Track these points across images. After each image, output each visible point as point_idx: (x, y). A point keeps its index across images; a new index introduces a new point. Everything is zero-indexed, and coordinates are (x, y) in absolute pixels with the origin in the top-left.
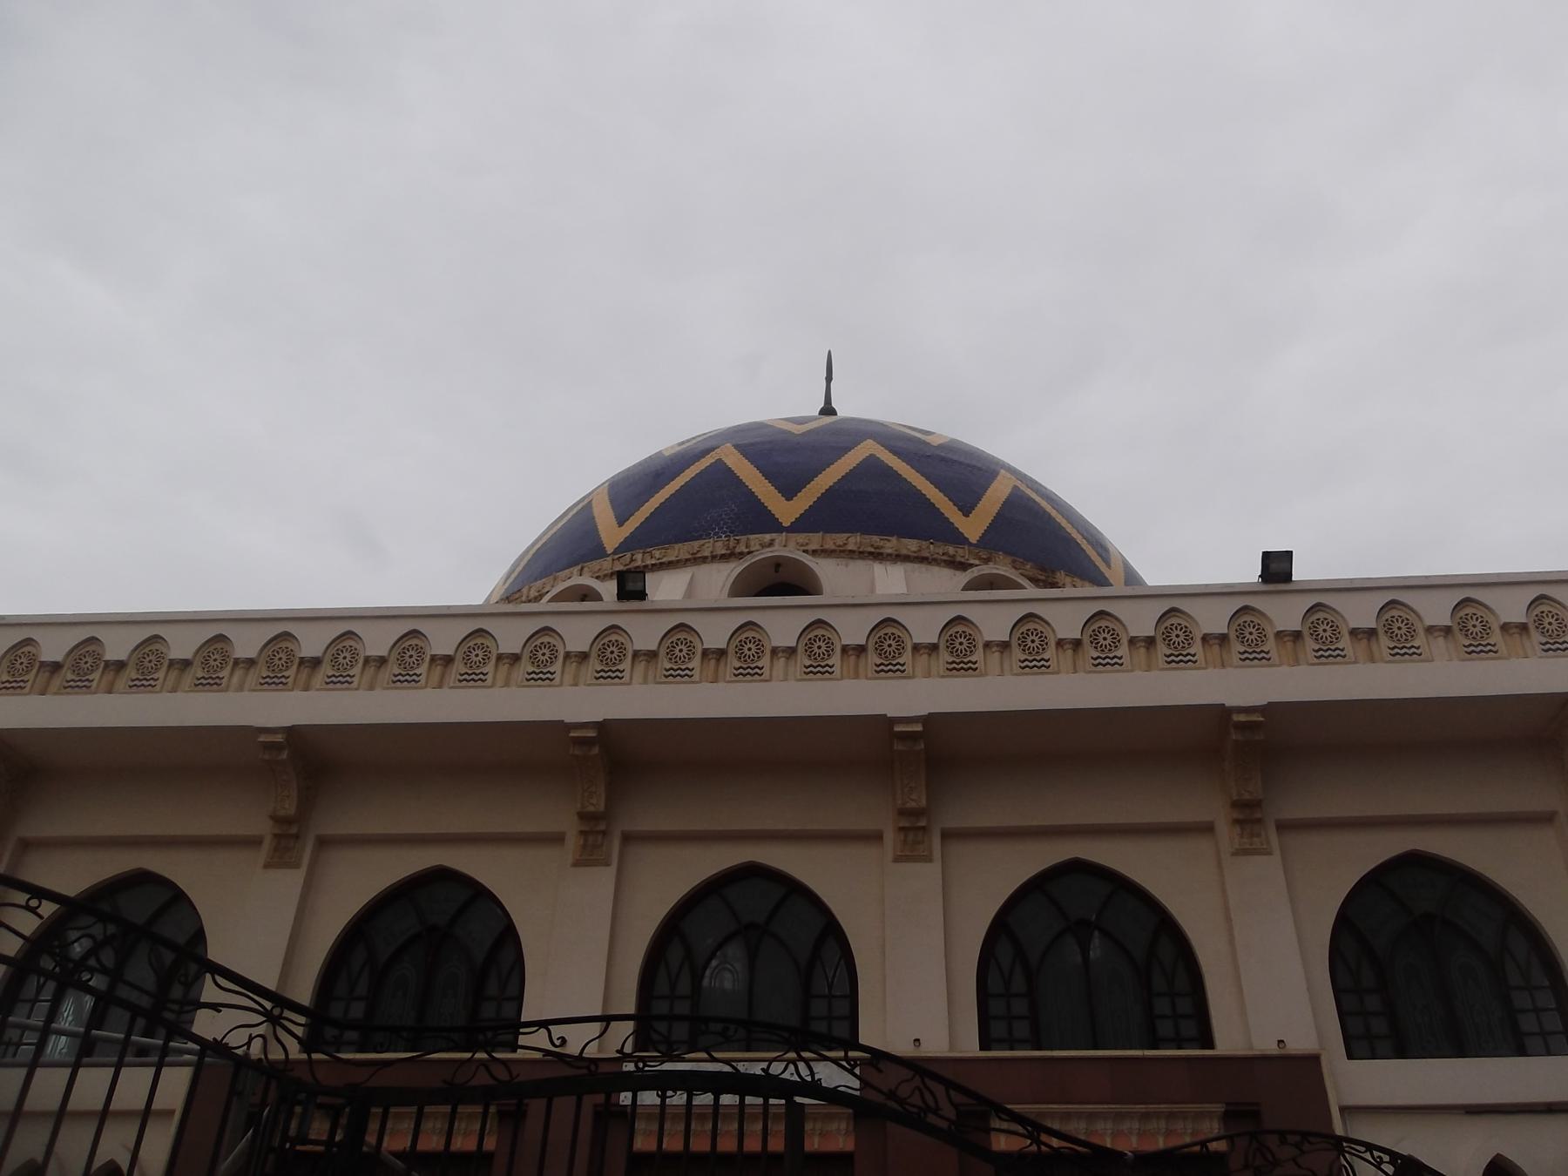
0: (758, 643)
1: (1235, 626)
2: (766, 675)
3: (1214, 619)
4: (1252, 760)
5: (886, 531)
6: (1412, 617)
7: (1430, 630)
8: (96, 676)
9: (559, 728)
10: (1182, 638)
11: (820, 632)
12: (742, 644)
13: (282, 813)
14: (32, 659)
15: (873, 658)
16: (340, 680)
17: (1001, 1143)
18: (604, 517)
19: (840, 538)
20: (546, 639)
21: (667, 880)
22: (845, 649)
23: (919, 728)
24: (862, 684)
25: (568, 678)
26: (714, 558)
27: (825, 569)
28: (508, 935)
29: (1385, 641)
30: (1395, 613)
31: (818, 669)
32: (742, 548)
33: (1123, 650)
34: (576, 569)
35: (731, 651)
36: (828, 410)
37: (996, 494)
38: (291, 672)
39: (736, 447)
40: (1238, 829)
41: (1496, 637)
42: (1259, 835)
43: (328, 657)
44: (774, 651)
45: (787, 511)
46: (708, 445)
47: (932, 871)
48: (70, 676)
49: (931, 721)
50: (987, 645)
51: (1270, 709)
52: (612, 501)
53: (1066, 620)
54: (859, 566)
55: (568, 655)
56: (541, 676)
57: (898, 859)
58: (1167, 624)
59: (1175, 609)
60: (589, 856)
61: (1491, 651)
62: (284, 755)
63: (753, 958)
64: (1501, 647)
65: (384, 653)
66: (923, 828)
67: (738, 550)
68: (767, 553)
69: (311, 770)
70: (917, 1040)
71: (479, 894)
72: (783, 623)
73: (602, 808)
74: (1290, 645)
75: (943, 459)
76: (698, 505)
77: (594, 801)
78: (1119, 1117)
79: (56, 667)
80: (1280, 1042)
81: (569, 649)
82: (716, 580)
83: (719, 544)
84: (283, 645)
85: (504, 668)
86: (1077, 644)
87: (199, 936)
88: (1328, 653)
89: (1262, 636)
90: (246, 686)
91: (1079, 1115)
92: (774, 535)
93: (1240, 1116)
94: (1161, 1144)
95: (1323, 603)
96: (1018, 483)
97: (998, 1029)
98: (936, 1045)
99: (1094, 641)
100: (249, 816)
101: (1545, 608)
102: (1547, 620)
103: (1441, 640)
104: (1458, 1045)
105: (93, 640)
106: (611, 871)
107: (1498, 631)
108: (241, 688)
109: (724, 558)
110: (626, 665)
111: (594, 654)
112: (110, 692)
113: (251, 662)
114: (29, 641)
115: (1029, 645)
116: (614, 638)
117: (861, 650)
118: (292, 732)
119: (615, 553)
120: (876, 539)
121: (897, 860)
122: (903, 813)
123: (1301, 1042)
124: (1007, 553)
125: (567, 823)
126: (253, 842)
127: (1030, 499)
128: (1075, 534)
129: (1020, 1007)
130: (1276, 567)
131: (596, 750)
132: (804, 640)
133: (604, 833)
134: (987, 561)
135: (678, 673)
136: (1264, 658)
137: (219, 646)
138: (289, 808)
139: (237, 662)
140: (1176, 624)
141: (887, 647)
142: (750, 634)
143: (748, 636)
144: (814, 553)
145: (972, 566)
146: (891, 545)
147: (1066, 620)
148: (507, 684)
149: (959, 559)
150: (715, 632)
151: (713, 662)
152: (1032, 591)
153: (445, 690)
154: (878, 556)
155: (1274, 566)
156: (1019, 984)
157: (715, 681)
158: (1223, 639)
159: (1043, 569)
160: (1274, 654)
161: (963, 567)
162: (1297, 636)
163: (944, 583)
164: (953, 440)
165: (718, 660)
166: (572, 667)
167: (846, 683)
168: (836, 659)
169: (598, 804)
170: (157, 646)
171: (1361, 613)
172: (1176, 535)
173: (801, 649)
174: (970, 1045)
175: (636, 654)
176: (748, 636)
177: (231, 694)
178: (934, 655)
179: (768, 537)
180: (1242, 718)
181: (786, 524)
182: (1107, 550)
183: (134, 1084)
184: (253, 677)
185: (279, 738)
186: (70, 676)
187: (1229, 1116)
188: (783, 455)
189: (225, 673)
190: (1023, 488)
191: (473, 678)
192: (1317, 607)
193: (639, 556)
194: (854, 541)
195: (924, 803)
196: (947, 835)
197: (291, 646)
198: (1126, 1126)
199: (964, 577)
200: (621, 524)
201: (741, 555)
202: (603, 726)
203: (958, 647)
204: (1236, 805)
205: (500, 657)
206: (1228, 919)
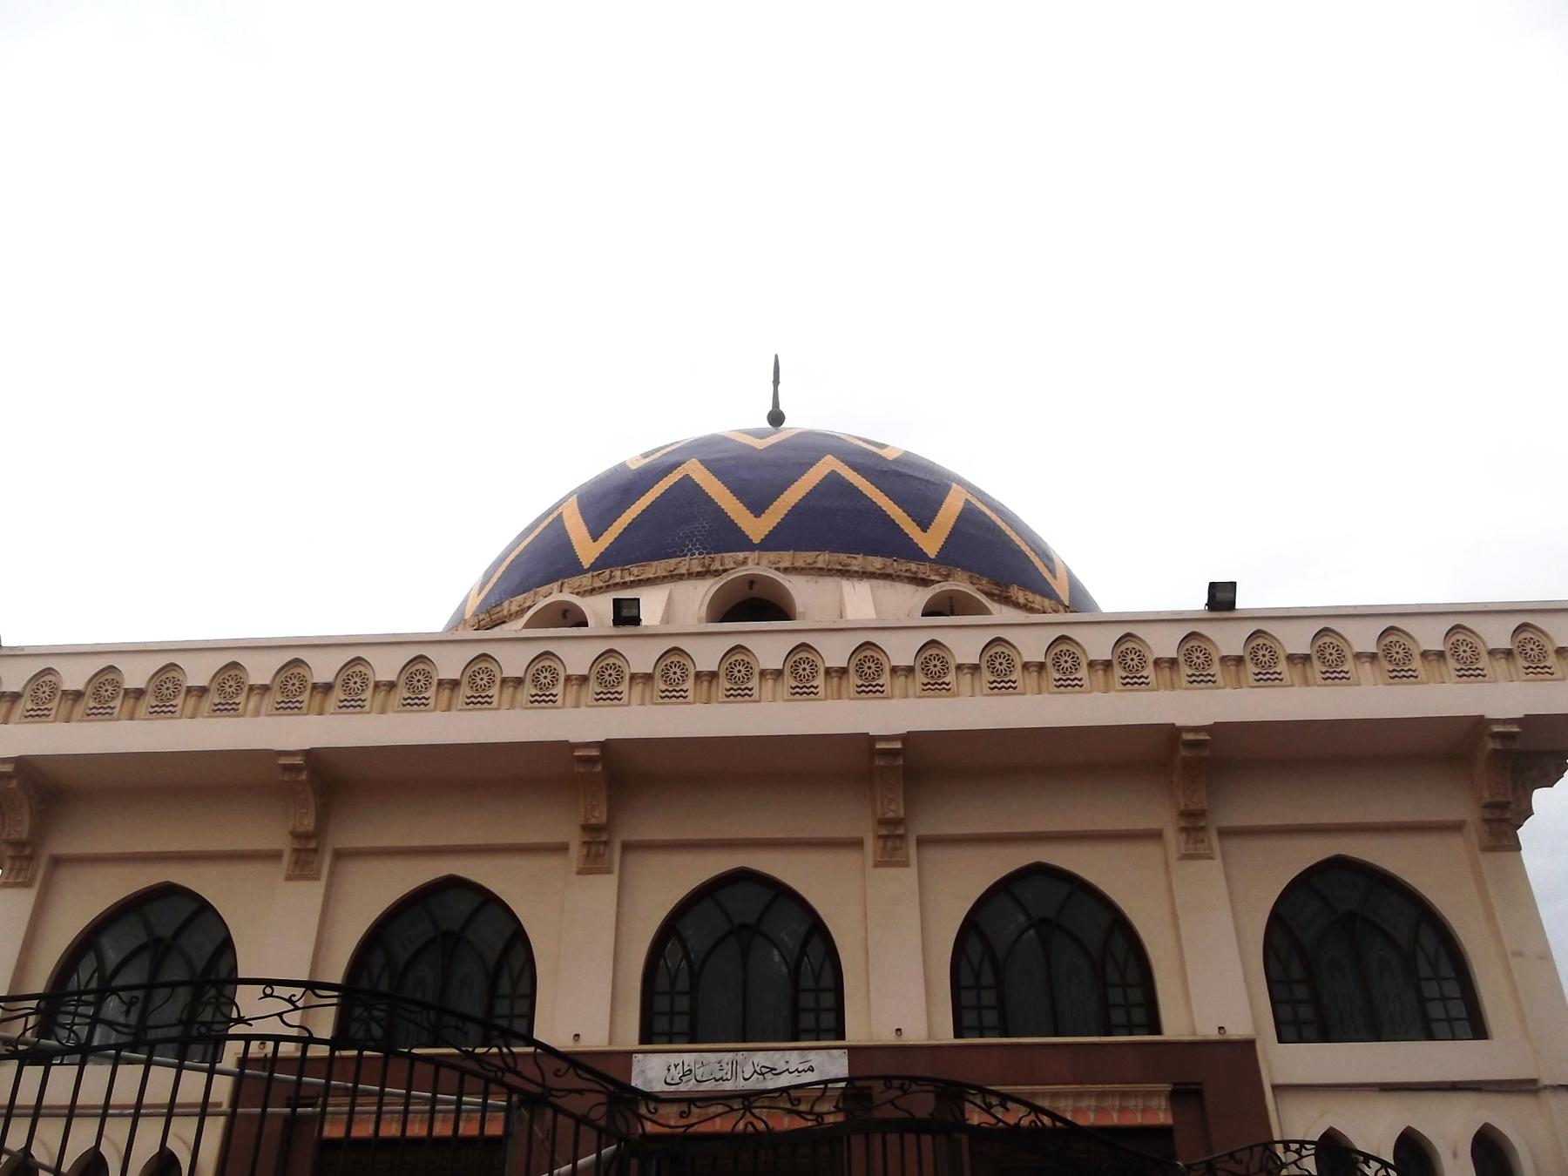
0: (747, 665)
1: (1183, 651)
2: (756, 696)
3: (1164, 644)
4: (1197, 772)
6: (1343, 645)
7: (1358, 656)
8: (117, 703)
11: (804, 655)
13: (301, 829)
14: (54, 688)
15: (854, 680)
16: (352, 704)
17: (975, 1118)
18: (577, 530)
20: (546, 663)
21: (664, 886)
23: (898, 745)
25: (570, 700)
26: (691, 575)
27: (800, 590)
28: (519, 938)
29: (1318, 666)
30: (1327, 640)
31: (803, 690)
32: (717, 566)
33: (1083, 672)
34: (556, 585)
36: (776, 418)
37: (951, 508)
38: (305, 697)
39: (702, 462)
40: (1183, 837)
41: (1417, 663)
44: (763, 673)
45: (756, 527)
46: (673, 459)
47: (909, 875)
50: (959, 667)
51: (1217, 729)
53: (1032, 645)
54: (829, 583)
55: (568, 679)
56: (544, 698)
58: (1123, 648)
59: (1129, 635)
60: (594, 863)
61: (1411, 676)
62: (303, 776)
63: (743, 957)
64: (1421, 673)
65: (393, 678)
67: (713, 568)
68: (742, 572)
69: (325, 795)
70: (899, 1030)
71: (488, 900)
72: (769, 646)
73: (604, 819)
74: (1232, 668)
78: (1078, 1096)
79: (78, 695)
80: (1221, 1028)
81: (570, 672)
82: (695, 597)
84: (295, 671)
85: (508, 691)
88: (1267, 677)
89: (1208, 660)
90: (263, 711)
91: (1067, 1095)
93: (1185, 1095)
95: (1262, 630)
96: (969, 497)
97: (970, 1018)
98: (916, 1034)
100: (271, 833)
101: (1461, 637)
102: (1462, 649)
104: (1375, 1031)
105: (112, 669)
107: (1418, 657)
108: (257, 714)
109: (700, 575)
113: (265, 689)
114: (49, 671)
115: (998, 668)
116: (611, 661)
118: (310, 754)
120: (843, 557)
121: (877, 865)
122: (883, 822)
123: (1238, 1029)
124: (964, 569)
125: (570, 833)
126: (275, 856)
128: (1024, 548)
129: (989, 997)
130: (1221, 597)
131: (599, 768)
132: (790, 662)
133: (606, 843)
134: (946, 577)
135: (674, 694)
136: (1210, 681)
137: (233, 673)
138: (308, 824)
139: (251, 688)
140: (1130, 651)
141: (867, 669)
143: (737, 660)
144: (786, 570)
145: (933, 582)
146: (857, 562)
147: (1032, 645)
148: (512, 707)
150: (707, 655)
151: (705, 684)
152: (1001, 613)
154: (845, 573)
155: (1220, 596)
156: (988, 977)
158: (1173, 662)
159: (998, 584)
160: (1219, 677)
161: (925, 583)
162: (1239, 660)
163: (907, 601)
164: (906, 453)
165: (710, 682)
167: (829, 703)
168: (819, 681)
169: (600, 816)
170: (174, 674)
171: (1297, 640)
172: (1127, 557)
173: (787, 671)
174: (945, 1034)
175: (633, 677)
176: (737, 660)
178: (910, 679)
179: (741, 555)
180: (1190, 736)
181: (756, 541)
182: (1051, 560)
183: (193, 1085)
184: (269, 702)
186: (92, 704)
188: (755, 471)
189: (241, 699)
190: (974, 501)
191: (480, 700)
192: (1258, 633)
193: (618, 573)
194: (823, 559)
196: (922, 842)
197: (303, 672)
198: (1084, 1104)
199: (922, 596)
200: (595, 539)
201: (717, 573)
202: (606, 746)
203: (932, 669)
204: (1182, 814)
205: (504, 681)
206: (1174, 914)
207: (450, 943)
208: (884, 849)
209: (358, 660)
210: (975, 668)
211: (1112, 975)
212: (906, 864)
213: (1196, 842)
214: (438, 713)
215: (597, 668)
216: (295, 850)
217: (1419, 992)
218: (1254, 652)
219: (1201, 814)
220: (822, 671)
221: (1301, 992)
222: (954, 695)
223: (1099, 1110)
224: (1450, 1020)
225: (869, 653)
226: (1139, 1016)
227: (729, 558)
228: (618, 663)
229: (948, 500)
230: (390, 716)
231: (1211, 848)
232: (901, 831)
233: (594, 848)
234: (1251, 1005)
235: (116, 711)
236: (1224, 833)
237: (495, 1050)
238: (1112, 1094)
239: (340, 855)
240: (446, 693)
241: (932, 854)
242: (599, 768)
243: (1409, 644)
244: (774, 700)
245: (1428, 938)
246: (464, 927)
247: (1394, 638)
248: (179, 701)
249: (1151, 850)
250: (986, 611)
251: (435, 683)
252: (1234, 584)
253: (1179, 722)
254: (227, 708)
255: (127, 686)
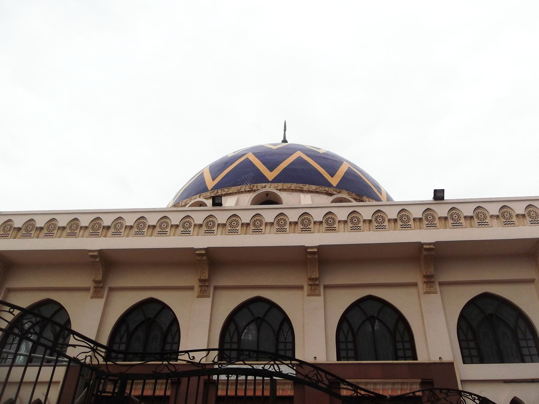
0: (261, 221)
3: (417, 212)
4: (431, 261)
5: (304, 183)
7: (492, 216)
8: (33, 232)
9: (192, 250)
10: (406, 219)
11: (282, 217)
12: (255, 221)
13: (97, 279)
14: (11, 226)
15: (300, 226)
16: (117, 234)
17: (344, 393)
18: (208, 178)
19: (289, 185)
20: (188, 220)
21: (229, 302)
22: (290, 223)
23: (316, 250)
24: (296, 235)
25: (195, 233)
26: (245, 192)
27: (283, 196)
28: (175, 321)
30: (480, 211)
31: (281, 230)
32: (255, 188)
33: (386, 223)
34: (198, 195)
35: (251, 223)
36: (285, 141)
38: (100, 231)
39: (253, 153)
42: (433, 287)
43: (113, 226)
44: (266, 224)
45: (271, 175)
46: (243, 153)
47: (320, 299)
48: (24, 232)
49: (320, 248)
50: (339, 222)
51: (437, 244)
52: (210, 172)
53: (367, 213)
54: (295, 194)
55: (195, 225)
56: (186, 232)
57: (308, 295)
58: (401, 214)
60: (203, 294)
61: (512, 224)
63: (259, 329)
64: (516, 222)
65: (132, 224)
66: (317, 285)
67: (254, 189)
68: (264, 190)
69: (107, 265)
70: (315, 357)
71: (165, 307)
72: (269, 214)
73: (207, 277)
74: (443, 221)
75: (324, 158)
76: (239, 174)
77: (204, 275)
78: (385, 384)
79: (19, 229)
80: (440, 358)
82: (246, 199)
83: (247, 187)
85: (173, 230)
86: (370, 221)
87: (69, 322)
89: (434, 218)
90: (85, 236)
92: (266, 184)
93: (426, 383)
94: (399, 393)
96: (350, 166)
97: (343, 354)
98: (322, 359)
99: (376, 221)
100: (86, 281)
103: (495, 220)
104: (501, 359)
105: (32, 220)
106: (210, 299)
107: (515, 217)
108: (83, 237)
109: (249, 192)
110: (215, 228)
111: (204, 225)
112: (38, 238)
113: (86, 228)
115: (354, 222)
116: (211, 219)
117: (296, 223)
119: (211, 190)
120: (301, 185)
121: (308, 295)
122: (310, 279)
123: (447, 358)
125: (195, 283)
126: (87, 289)
127: (354, 171)
128: (369, 184)
129: (351, 346)
130: (439, 195)
131: (205, 258)
132: (277, 220)
133: (208, 286)
134: (339, 193)
135: (233, 231)
137: (75, 222)
138: (99, 278)
139: (81, 227)
140: (403, 216)
141: (305, 222)
142: (258, 218)
143: (257, 219)
144: (280, 190)
145: (334, 194)
146: (306, 187)
147: (367, 213)
148: (174, 235)
149: (330, 192)
150: (246, 217)
151: (245, 227)
153: (153, 237)
154: (302, 191)
155: (438, 195)
156: (350, 338)
157: (246, 234)
158: (420, 219)
159: (359, 196)
160: (438, 225)
161: (331, 195)
162: (446, 218)
163: (325, 200)
165: (247, 227)
166: (197, 229)
168: (287, 226)
169: (206, 276)
171: (468, 211)
172: (403, 183)
173: (275, 223)
174: (333, 359)
175: (219, 225)
176: (257, 219)
177: (79, 239)
178: (321, 225)
179: (264, 184)
180: (427, 247)
181: (270, 180)
182: (380, 189)
185: (96, 254)
186: (24, 232)
187: (422, 384)
188: (270, 157)
189: (77, 231)
190: (352, 167)
191: (163, 233)
192: (453, 208)
194: (293, 186)
195: (317, 276)
196: (326, 287)
198: (387, 387)
200: (213, 180)
203: (329, 222)
205: (172, 226)
206: (422, 316)
207: (150, 323)
208: (311, 289)
209: (120, 218)
210: (345, 222)
211: (398, 338)
212: (319, 295)
213: (430, 287)
214: (148, 237)
215: (206, 221)
216: (95, 287)
217: (518, 344)
218: (452, 216)
219: (432, 276)
220: (288, 223)
221: (472, 344)
222: (337, 232)
223: (393, 390)
224: (531, 355)
225: (306, 217)
226: (409, 353)
227: (260, 185)
228: (213, 220)
229: (342, 167)
230: (130, 238)
231: (436, 289)
232: (317, 283)
233: (203, 288)
234: (452, 349)
235: (32, 235)
236: (441, 284)
237: (165, 363)
238: (398, 383)
239: (111, 289)
240: (151, 230)
241: (330, 292)
242: (205, 258)
243: (512, 212)
244: (270, 233)
245: (522, 325)
246: (156, 316)
247: (505, 210)
248: (55, 232)
249: (413, 290)
250: (351, 202)
251: (147, 226)
252: (443, 190)
253: (423, 241)
254: (72, 234)
255: (37, 226)
